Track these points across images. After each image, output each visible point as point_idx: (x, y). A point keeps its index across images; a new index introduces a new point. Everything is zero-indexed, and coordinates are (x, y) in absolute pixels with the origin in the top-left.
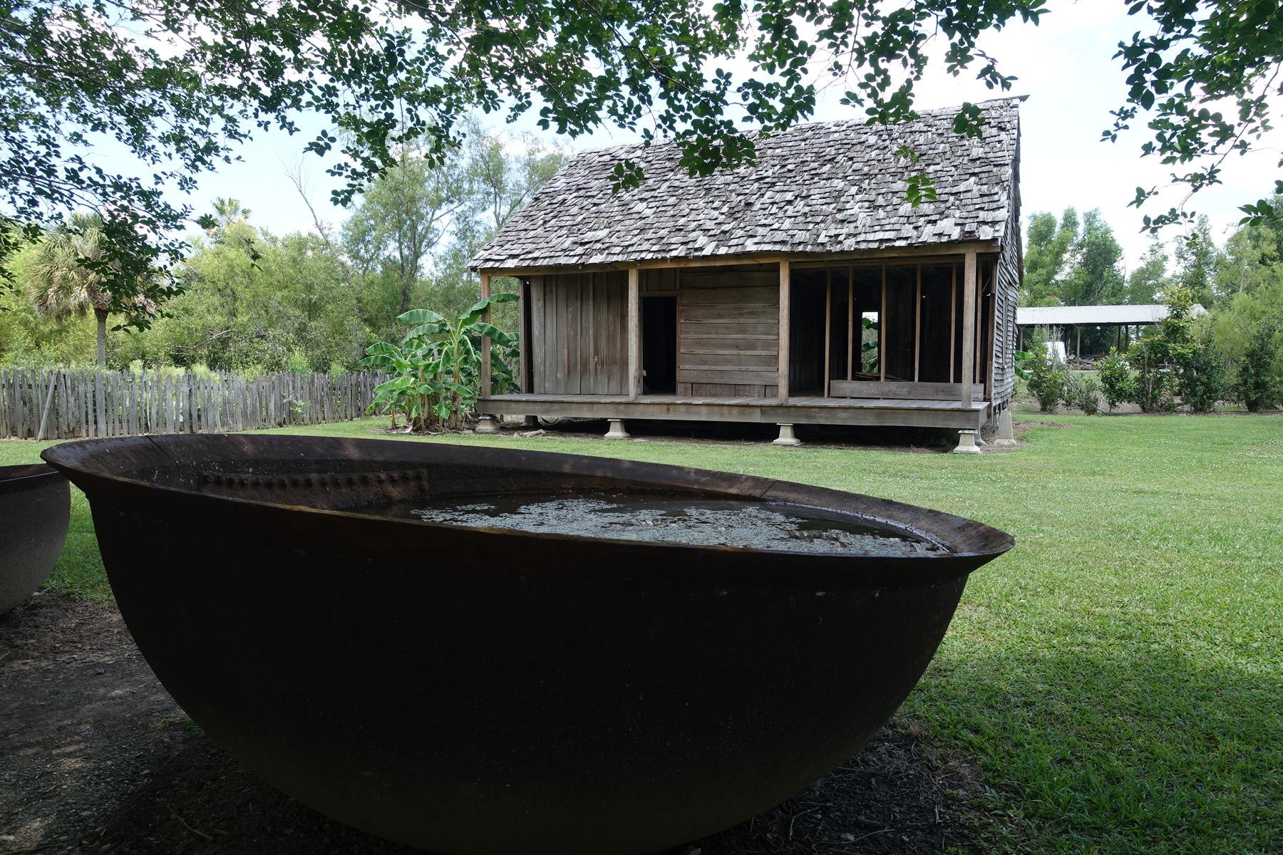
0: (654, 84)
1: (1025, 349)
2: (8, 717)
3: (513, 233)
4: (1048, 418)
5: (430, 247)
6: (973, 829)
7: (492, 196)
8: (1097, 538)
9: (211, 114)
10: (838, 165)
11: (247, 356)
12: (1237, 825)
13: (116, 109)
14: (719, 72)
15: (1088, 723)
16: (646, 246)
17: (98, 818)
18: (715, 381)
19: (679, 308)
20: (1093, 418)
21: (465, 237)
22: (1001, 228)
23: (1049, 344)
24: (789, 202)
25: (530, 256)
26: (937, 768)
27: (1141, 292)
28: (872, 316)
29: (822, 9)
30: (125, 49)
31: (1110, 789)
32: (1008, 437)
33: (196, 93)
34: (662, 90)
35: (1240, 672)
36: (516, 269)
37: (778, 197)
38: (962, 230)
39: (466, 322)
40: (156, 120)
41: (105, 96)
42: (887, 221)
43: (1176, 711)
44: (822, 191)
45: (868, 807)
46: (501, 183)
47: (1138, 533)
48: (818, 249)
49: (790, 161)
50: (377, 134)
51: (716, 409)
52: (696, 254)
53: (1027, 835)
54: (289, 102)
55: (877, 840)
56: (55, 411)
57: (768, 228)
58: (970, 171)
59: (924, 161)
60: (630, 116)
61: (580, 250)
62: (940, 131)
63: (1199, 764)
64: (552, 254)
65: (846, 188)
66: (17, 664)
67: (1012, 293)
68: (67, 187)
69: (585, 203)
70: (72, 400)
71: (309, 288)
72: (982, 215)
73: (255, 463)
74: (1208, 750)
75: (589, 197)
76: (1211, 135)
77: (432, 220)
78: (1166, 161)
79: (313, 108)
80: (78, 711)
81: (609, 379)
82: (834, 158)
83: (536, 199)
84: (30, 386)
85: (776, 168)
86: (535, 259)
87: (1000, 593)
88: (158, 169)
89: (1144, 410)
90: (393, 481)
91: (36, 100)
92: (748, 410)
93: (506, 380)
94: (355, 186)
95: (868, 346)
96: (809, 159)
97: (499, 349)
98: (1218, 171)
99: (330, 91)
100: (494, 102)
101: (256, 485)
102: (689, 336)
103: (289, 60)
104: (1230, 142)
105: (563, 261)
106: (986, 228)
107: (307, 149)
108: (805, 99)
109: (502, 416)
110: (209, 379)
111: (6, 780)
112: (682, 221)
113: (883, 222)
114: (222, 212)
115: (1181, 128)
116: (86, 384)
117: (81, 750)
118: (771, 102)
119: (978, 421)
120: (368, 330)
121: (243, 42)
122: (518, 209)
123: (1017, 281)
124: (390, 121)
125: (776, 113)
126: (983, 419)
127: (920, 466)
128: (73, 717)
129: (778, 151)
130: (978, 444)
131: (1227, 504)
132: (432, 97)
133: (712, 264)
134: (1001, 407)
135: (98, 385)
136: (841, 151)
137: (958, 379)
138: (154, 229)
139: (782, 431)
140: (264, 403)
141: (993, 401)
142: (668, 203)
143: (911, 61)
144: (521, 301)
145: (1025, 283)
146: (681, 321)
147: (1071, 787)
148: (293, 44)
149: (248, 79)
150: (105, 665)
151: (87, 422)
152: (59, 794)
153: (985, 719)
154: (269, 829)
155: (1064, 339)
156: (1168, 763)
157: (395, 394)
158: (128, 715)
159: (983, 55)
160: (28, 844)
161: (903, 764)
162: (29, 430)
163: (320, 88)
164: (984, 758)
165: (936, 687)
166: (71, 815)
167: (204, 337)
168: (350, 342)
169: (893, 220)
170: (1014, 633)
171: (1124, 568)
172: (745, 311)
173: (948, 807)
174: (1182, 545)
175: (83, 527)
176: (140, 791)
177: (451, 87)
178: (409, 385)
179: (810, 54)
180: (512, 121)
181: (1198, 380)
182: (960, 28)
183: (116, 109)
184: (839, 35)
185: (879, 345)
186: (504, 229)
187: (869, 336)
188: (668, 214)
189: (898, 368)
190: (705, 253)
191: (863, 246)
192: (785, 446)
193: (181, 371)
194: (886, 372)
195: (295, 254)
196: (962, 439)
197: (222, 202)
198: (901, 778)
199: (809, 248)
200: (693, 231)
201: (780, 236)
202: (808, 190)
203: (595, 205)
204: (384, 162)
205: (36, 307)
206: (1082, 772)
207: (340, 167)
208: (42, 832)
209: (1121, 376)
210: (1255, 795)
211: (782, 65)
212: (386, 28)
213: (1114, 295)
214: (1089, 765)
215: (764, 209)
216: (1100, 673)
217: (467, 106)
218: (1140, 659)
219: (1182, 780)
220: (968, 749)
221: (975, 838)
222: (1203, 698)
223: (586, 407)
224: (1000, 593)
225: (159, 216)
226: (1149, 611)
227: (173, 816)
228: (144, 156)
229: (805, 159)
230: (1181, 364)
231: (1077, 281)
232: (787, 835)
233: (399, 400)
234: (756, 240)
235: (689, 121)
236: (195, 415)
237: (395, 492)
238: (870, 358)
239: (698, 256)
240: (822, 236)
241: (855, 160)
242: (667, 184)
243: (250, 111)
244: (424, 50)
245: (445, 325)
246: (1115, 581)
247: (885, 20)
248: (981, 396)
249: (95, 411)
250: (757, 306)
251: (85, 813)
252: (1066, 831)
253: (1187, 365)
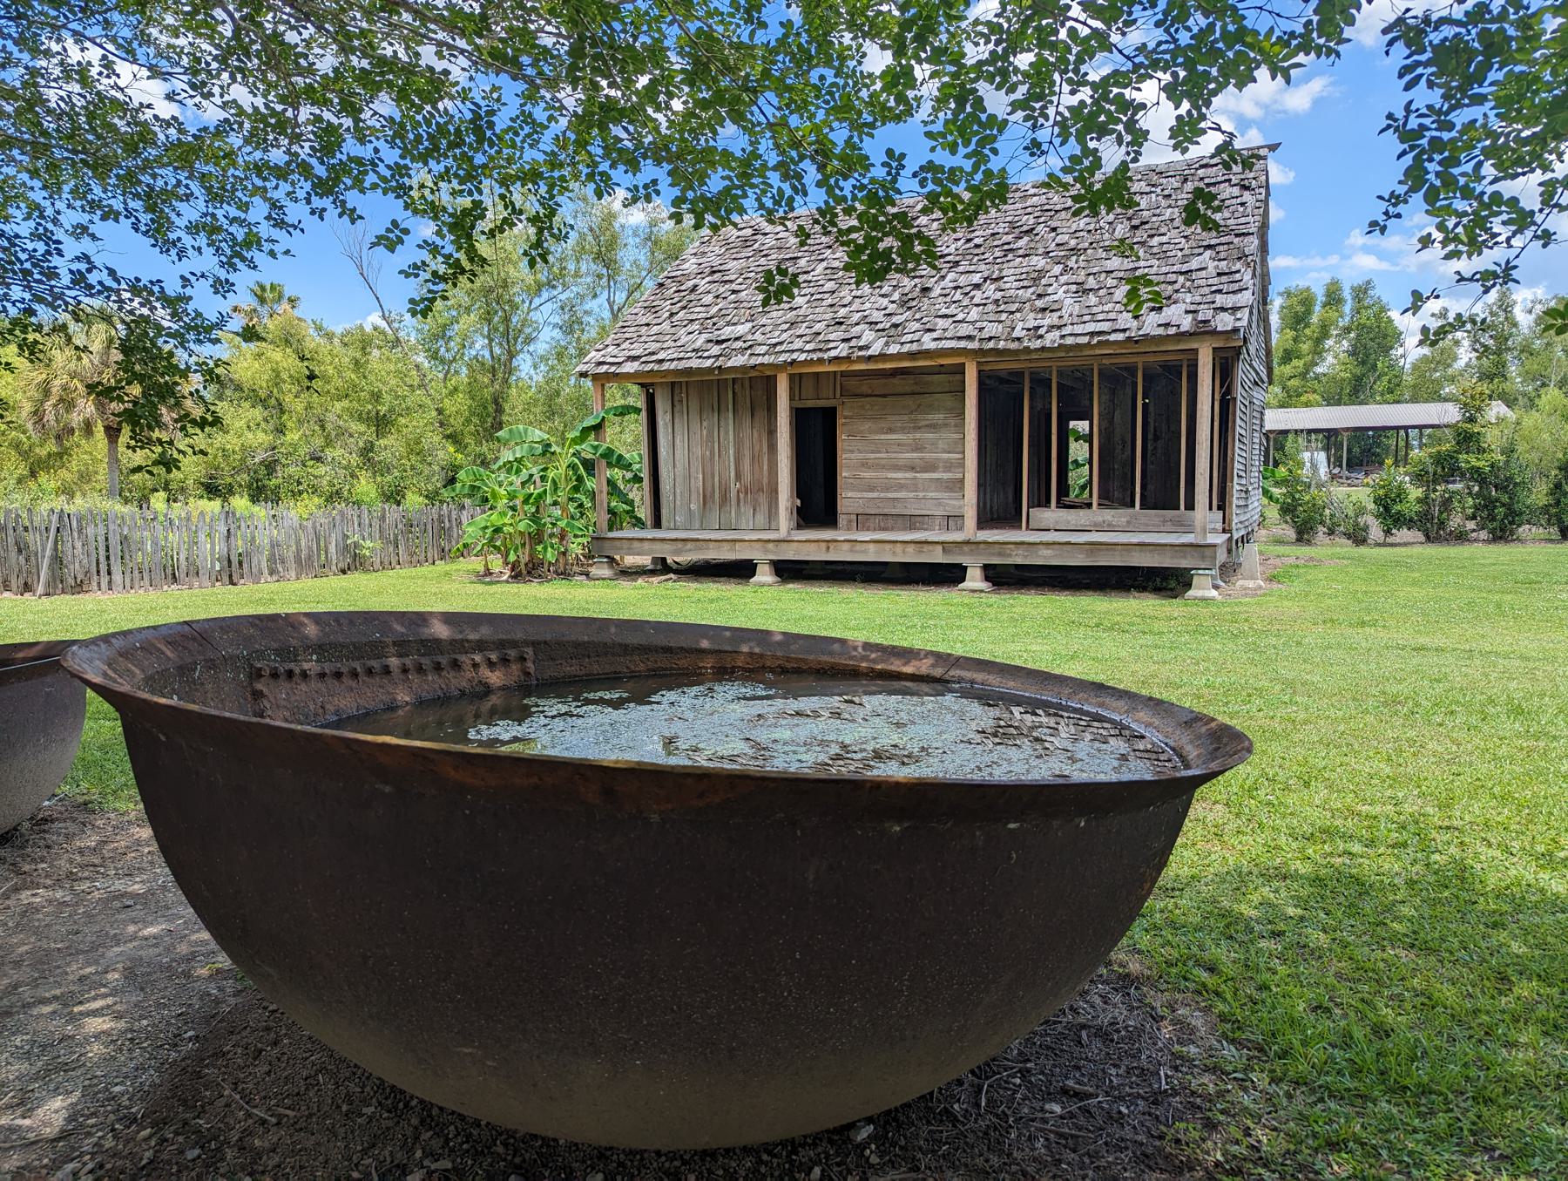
0: (811, 173)
1: (1276, 464)
2: (17, 964)
3: (632, 329)
4: (1304, 551)
5: (528, 344)
6: (1208, 1098)
7: (605, 280)
8: (1366, 712)
9: (251, 196)
10: (1038, 238)
11: (299, 483)
12: (1535, 1091)
13: (131, 193)
14: (890, 153)
15: (1351, 959)
16: (798, 344)
17: (133, 1096)
18: (886, 511)
19: (840, 421)
20: (1363, 550)
21: (572, 332)
22: (1244, 315)
23: (1306, 455)
24: (977, 286)
25: (654, 358)
26: (1163, 1018)
27: (1426, 391)
28: (1082, 426)
29: (1016, 75)
30: (142, 117)
31: (1377, 1045)
32: (1253, 578)
33: (231, 171)
34: (819, 176)
35: (1542, 891)
36: (637, 374)
37: (963, 280)
38: (1194, 319)
39: (575, 441)
40: (182, 207)
41: (117, 176)
42: (1100, 309)
43: (1461, 942)
44: (1018, 271)
45: (1078, 1068)
46: (616, 262)
47: (1417, 705)
48: (1014, 346)
49: (977, 233)
50: (462, 225)
52: (860, 353)
53: (1274, 1105)
54: (349, 182)
55: (1089, 1112)
56: (57, 560)
57: (951, 320)
58: (1205, 243)
59: (1146, 231)
60: (781, 210)
61: (716, 350)
62: (1166, 192)
63: (1488, 1012)
64: (681, 355)
65: (1048, 267)
66: (25, 896)
67: (1258, 394)
68: (73, 293)
69: (722, 290)
70: (78, 545)
71: (376, 397)
72: (1220, 300)
73: (321, 649)
74: (1500, 994)
75: (726, 282)
76: (1504, 223)
77: (530, 310)
78: (1447, 257)
79: (380, 191)
80: (103, 956)
82: (1033, 229)
83: (661, 285)
84: (26, 529)
85: (960, 243)
86: (661, 361)
87: (1242, 787)
88: (185, 267)
89: (1428, 539)
90: (491, 665)
91: (30, 183)
92: (926, 548)
93: (628, 512)
94: (437, 292)
95: (1077, 464)
96: (1001, 230)
97: (617, 474)
98: (1515, 267)
99: (400, 170)
100: (607, 185)
101: (322, 675)
102: (853, 456)
103: (348, 129)
104: (1529, 233)
106: (1225, 316)
107: (374, 245)
108: (996, 185)
109: (622, 558)
110: (251, 516)
111: (16, 1047)
112: (843, 312)
113: (1095, 310)
114: (262, 300)
115: (1469, 215)
116: (96, 525)
117: (108, 1007)
118: (956, 190)
119: (1215, 558)
120: (452, 449)
121: (290, 110)
122: (637, 295)
123: (1265, 379)
124: (478, 211)
125: (962, 202)
126: (1222, 556)
127: (1143, 616)
128: (97, 962)
130: (1216, 587)
131: (1531, 665)
132: (532, 176)
133: (881, 366)
134: (1245, 539)
135: (111, 527)
136: (1042, 220)
137: (1190, 506)
138: (183, 344)
140: (322, 544)
141: (1234, 532)
142: (825, 289)
143: (1128, 138)
144: (644, 414)
145: (1276, 378)
146: (842, 438)
147: (1330, 1044)
148: (351, 108)
149: (297, 155)
150: (134, 896)
151: (98, 572)
152: (84, 1065)
153: (1223, 954)
154: (345, 1108)
155: (1327, 449)
156: (1449, 1011)
157: (489, 531)
158: (164, 960)
159: (1219, 129)
160: (48, 1130)
161: (1121, 1013)
162: (26, 584)
163: (388, 167)
164: (1221, 1007)
165: (1162, 911)
166: (99, 1092)
167: (243, 460)
168: (430, 464)
169: (1106, 308)
170: (1259, 840)
171: (1399, 752)
172: (924, 423)
173: (1176, 1068)
174: (1474, 720)
175: (99, 712)
176: (183, 1060)
177: (554, 164)
178: (506, 521)
179: (1000, 131)
180: (630, 205)
181: (1497, 500)
182: (1188, 95)
183: (131, 193)
184: (1037, 105)
185: (1090, 462)
186: (621, 324)
187: (1078, 451)
188: (824, 303)
189: (1115, 491)
190: (870, 352)
191: (1069, 341)
192: (974, 591)
193: (215, 506)
194: (1100, 497)
195: (358, 355)
196: (1195, 580)
197: (263, 288)
198: (1118, 1031)
199: (1002, 344)
200: (857, 324)
201: (965, 330)
202: (1001, 270)
203: (734, 292)
204: (471, 260)
205: (30, 426)
206: (1343, 1023)
207: (415, 266)
208: (64, 1114)
209: (1399, 496)
210: (1558, 1052)
211: (967, 144)
212: (470, 89)
213: (1391, 391)
214: (1352, 1014)
215: (945, 295)
216: (1367, 893)
217: (573, 185)
218: (1417, 873)
219: (1467, 1033)
220: (1200, 993)
221: (1210, 1110)
222: (1495, 925)
223: (726, 546)
224: (1242, 787)
225: (188, 328)
226: (1430, 810)
227: (226, 1093)
228: (168, 250)
229: (996, 230)
230: (1476, 481)
231: (1342, 374)
232: (978, 1105)
233: (492, 539)
234: (935, 335)
235: (854, 215)
236: (235, 560)
237: (495, 678)
238: (1080, 477)
239: (863, 357)
240: (1018, 328)
241: (1059, 231)
242: (824, 264)
243: (301, 194)
244: (518, 117)
245: (549, 445)
246: (1388, 770)
247: (1094, 86)
248: (1219, 526)
249: (108, 558)
250: (938, 417)
251: (117, 1089)
252: (1321, 1100)
253: (1483, 482)
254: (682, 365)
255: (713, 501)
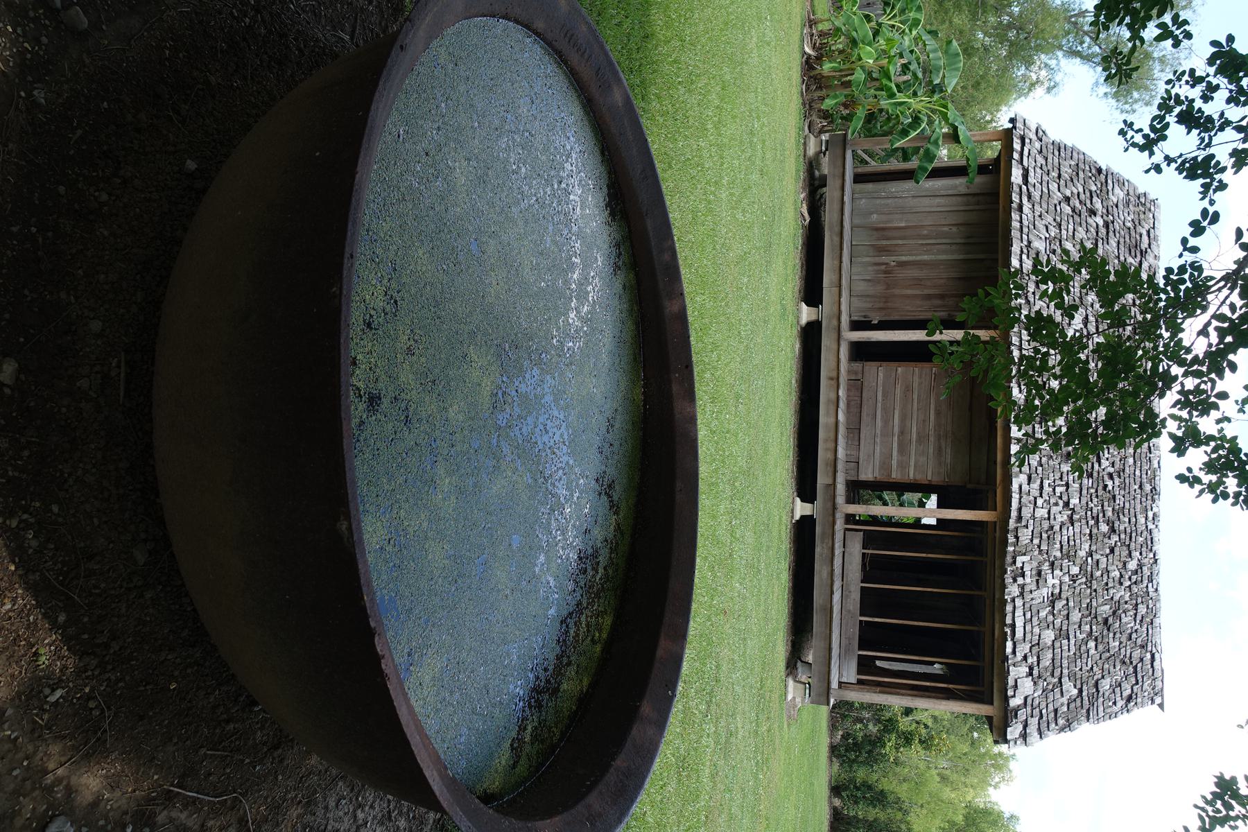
3: (1056, 160)
24: (1067, 504)
25: (1025, 200)
48: (1009, 559)
51: (832, 435)
64: (1025, 230)
81: (869, 280)
92: (830, 469)
102: (916, 379)
105: (1015, 248)
129: (1131, 461)
139: (808, 506)
201: (1026, 513)
254: (1015, 234)
255: (879, 239)
